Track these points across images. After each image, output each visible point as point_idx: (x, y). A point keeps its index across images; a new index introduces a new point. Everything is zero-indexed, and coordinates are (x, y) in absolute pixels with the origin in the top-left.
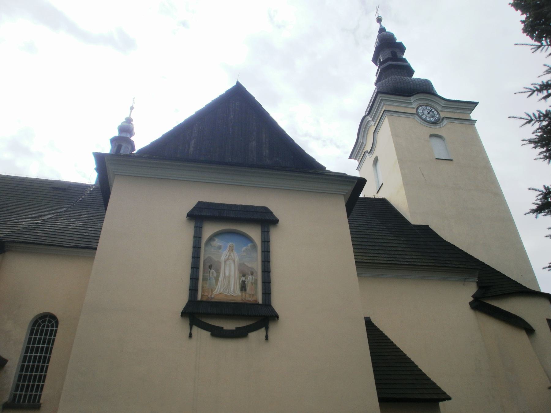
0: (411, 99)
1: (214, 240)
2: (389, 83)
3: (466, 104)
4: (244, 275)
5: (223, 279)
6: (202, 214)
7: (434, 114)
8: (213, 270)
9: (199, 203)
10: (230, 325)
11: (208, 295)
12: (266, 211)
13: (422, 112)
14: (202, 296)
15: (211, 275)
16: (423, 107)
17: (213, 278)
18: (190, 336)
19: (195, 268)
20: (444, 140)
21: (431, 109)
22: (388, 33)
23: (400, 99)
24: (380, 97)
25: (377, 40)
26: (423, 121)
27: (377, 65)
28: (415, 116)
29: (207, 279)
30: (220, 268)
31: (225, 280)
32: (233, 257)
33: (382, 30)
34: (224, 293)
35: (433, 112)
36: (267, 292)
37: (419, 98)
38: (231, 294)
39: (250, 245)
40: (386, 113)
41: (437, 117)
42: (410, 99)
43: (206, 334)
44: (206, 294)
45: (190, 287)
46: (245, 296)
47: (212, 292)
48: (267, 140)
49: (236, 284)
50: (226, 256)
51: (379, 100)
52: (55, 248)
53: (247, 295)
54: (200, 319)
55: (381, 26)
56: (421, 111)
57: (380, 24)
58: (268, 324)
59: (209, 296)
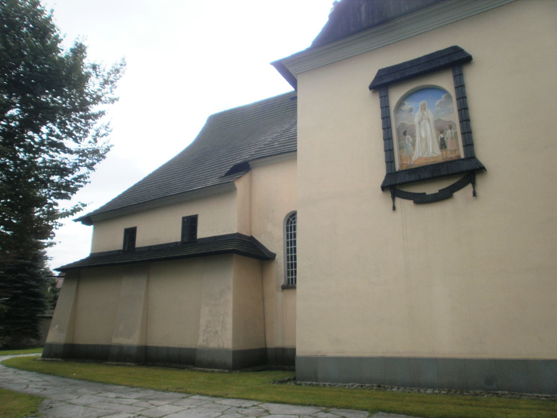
1: (404, 104)
4: (442, 132)
6: (384, 82)
9: (380, 71)
10: (431, 189)
12: (456, 50)
14: (401, 165)
15: (407, 141)
18: (394, 208)
30: (415, 130)
32: (427, 116)
36: (469, 144)
38: (431, 156)
39: (443, 97)
43: (409, 203)
44: (405, 162)
45: (386, 159)
46: (446, 153)
47: (411, 159)
52: (287, 154)
53: (448, 152)
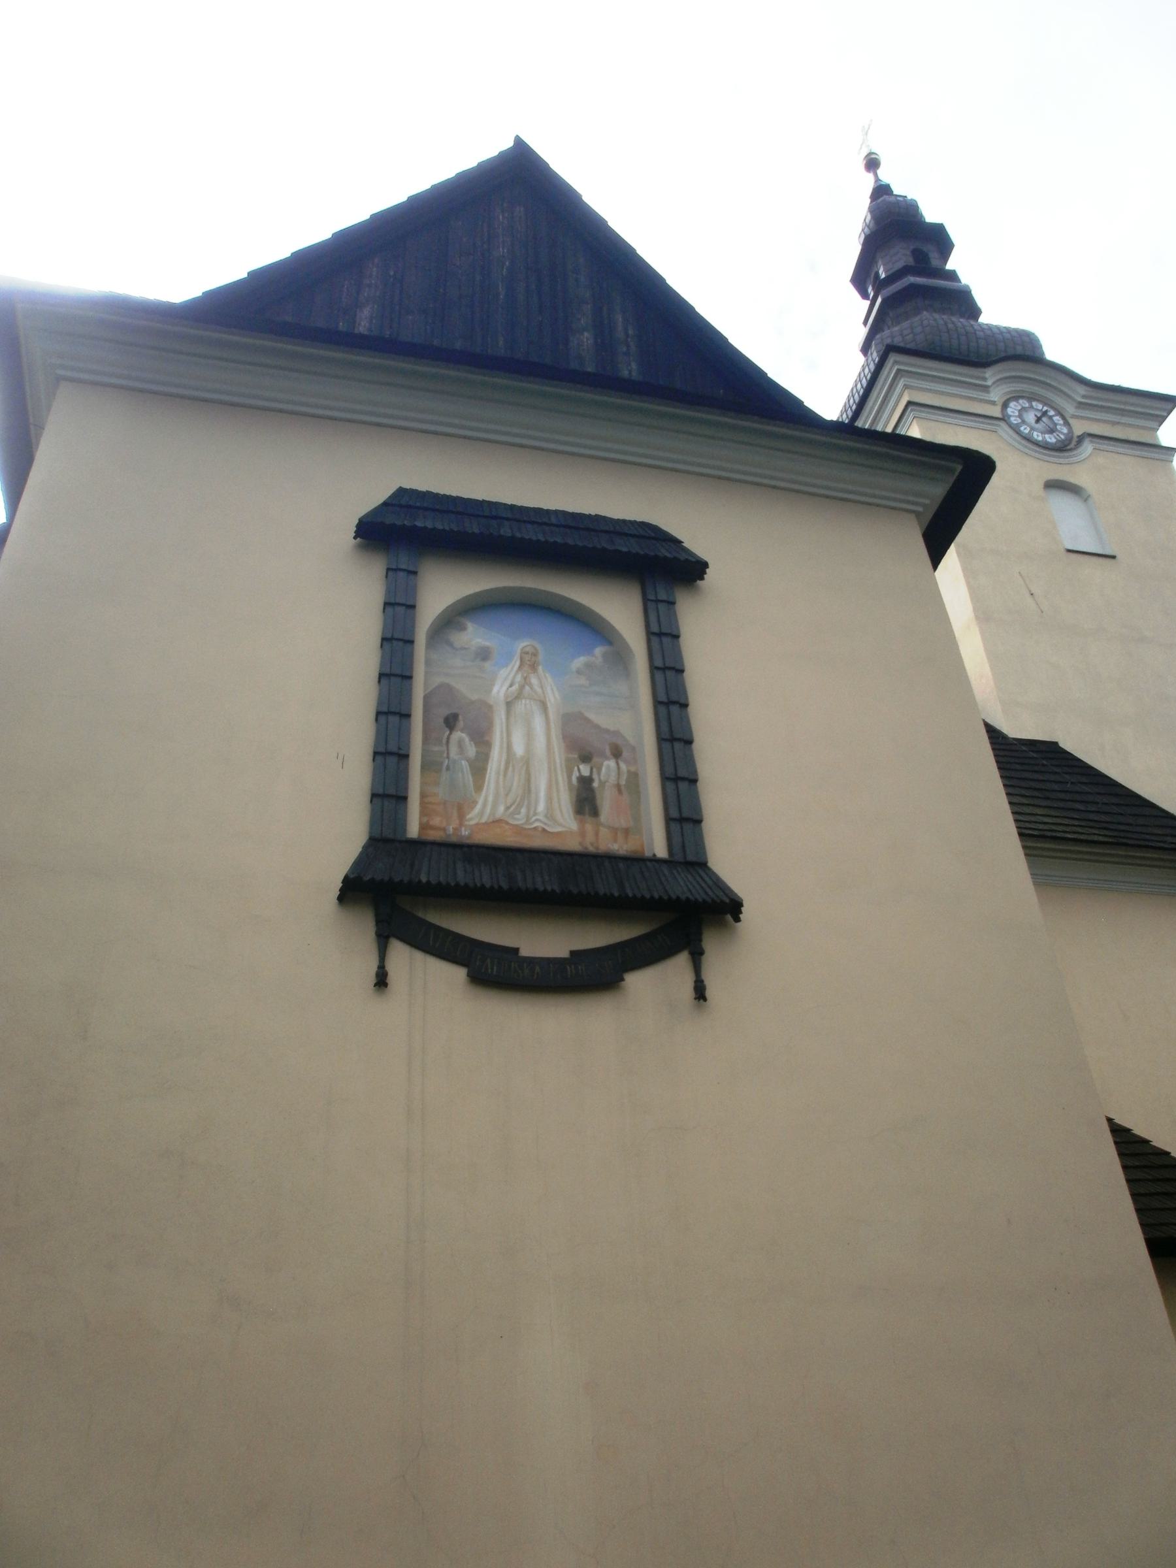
0: (987, 375)
1: (463, 629)
2: (912, 332)
3: (1148, 402)
4: (586, 758)
5: (502, 767)
6: (419, 524)
7: (1056, 425)
8: (464, 735)
9: (401, 492)
11: (444, 824)
13: (1020, 416)
14: (423, 827)
15: (454, 750)
16: (1021, 401)
17: (463, 762)
18: (381, 981)
19: (394, 713)
20: (1086, 500)
21: (1045, 408)
22: (901, 199)
23: (955, 373)
24: (896, 362)
25: (869, 217)
26: (1024, 442)
27: (865, 295)
28: (999, 426)
29: (442, 763)
31: (513, 771)
32: (539, 690)
33: (881, 191)
34: (511, 821)
35: (1051, 418)
37: (1013, 374)
39: (599, 651)
40: (912, 411)
41: (1062, 433)
42: (982, 375)
44: (436, 821)
46: (597, 834)
48: (631, 332)
49: (558, 791)
50: (511, 686)
51: (889, 373)
53: (604, 832)
54: (420, 914)
55: (877, 179)
56: (1017, 414)
57: (876, 175)
58: (700, 940)
59: (451, 830)
